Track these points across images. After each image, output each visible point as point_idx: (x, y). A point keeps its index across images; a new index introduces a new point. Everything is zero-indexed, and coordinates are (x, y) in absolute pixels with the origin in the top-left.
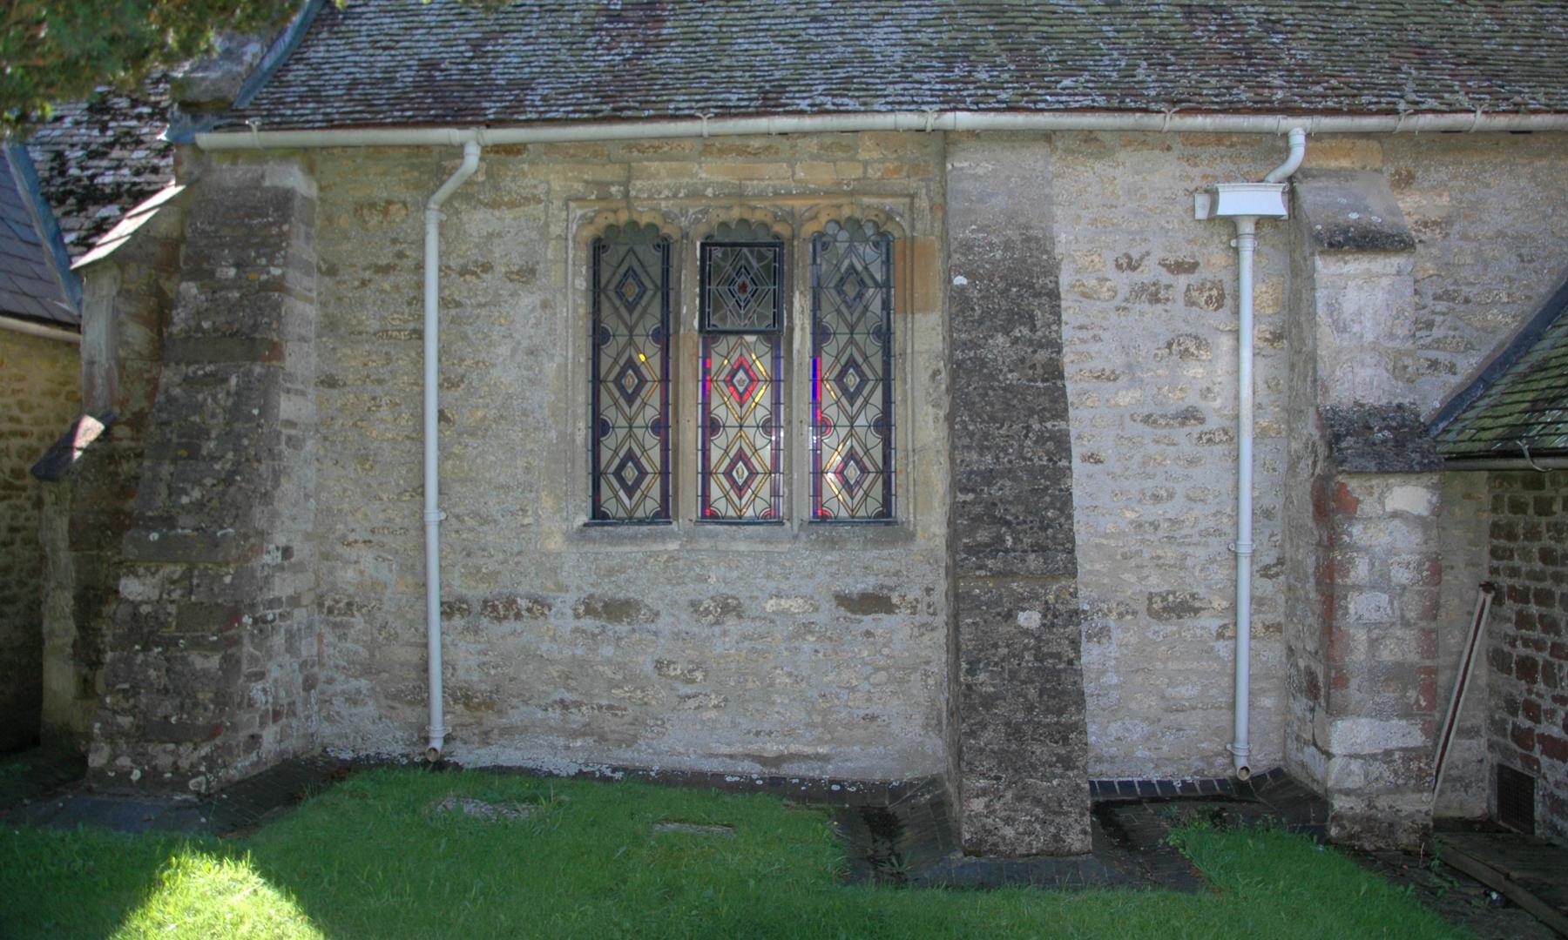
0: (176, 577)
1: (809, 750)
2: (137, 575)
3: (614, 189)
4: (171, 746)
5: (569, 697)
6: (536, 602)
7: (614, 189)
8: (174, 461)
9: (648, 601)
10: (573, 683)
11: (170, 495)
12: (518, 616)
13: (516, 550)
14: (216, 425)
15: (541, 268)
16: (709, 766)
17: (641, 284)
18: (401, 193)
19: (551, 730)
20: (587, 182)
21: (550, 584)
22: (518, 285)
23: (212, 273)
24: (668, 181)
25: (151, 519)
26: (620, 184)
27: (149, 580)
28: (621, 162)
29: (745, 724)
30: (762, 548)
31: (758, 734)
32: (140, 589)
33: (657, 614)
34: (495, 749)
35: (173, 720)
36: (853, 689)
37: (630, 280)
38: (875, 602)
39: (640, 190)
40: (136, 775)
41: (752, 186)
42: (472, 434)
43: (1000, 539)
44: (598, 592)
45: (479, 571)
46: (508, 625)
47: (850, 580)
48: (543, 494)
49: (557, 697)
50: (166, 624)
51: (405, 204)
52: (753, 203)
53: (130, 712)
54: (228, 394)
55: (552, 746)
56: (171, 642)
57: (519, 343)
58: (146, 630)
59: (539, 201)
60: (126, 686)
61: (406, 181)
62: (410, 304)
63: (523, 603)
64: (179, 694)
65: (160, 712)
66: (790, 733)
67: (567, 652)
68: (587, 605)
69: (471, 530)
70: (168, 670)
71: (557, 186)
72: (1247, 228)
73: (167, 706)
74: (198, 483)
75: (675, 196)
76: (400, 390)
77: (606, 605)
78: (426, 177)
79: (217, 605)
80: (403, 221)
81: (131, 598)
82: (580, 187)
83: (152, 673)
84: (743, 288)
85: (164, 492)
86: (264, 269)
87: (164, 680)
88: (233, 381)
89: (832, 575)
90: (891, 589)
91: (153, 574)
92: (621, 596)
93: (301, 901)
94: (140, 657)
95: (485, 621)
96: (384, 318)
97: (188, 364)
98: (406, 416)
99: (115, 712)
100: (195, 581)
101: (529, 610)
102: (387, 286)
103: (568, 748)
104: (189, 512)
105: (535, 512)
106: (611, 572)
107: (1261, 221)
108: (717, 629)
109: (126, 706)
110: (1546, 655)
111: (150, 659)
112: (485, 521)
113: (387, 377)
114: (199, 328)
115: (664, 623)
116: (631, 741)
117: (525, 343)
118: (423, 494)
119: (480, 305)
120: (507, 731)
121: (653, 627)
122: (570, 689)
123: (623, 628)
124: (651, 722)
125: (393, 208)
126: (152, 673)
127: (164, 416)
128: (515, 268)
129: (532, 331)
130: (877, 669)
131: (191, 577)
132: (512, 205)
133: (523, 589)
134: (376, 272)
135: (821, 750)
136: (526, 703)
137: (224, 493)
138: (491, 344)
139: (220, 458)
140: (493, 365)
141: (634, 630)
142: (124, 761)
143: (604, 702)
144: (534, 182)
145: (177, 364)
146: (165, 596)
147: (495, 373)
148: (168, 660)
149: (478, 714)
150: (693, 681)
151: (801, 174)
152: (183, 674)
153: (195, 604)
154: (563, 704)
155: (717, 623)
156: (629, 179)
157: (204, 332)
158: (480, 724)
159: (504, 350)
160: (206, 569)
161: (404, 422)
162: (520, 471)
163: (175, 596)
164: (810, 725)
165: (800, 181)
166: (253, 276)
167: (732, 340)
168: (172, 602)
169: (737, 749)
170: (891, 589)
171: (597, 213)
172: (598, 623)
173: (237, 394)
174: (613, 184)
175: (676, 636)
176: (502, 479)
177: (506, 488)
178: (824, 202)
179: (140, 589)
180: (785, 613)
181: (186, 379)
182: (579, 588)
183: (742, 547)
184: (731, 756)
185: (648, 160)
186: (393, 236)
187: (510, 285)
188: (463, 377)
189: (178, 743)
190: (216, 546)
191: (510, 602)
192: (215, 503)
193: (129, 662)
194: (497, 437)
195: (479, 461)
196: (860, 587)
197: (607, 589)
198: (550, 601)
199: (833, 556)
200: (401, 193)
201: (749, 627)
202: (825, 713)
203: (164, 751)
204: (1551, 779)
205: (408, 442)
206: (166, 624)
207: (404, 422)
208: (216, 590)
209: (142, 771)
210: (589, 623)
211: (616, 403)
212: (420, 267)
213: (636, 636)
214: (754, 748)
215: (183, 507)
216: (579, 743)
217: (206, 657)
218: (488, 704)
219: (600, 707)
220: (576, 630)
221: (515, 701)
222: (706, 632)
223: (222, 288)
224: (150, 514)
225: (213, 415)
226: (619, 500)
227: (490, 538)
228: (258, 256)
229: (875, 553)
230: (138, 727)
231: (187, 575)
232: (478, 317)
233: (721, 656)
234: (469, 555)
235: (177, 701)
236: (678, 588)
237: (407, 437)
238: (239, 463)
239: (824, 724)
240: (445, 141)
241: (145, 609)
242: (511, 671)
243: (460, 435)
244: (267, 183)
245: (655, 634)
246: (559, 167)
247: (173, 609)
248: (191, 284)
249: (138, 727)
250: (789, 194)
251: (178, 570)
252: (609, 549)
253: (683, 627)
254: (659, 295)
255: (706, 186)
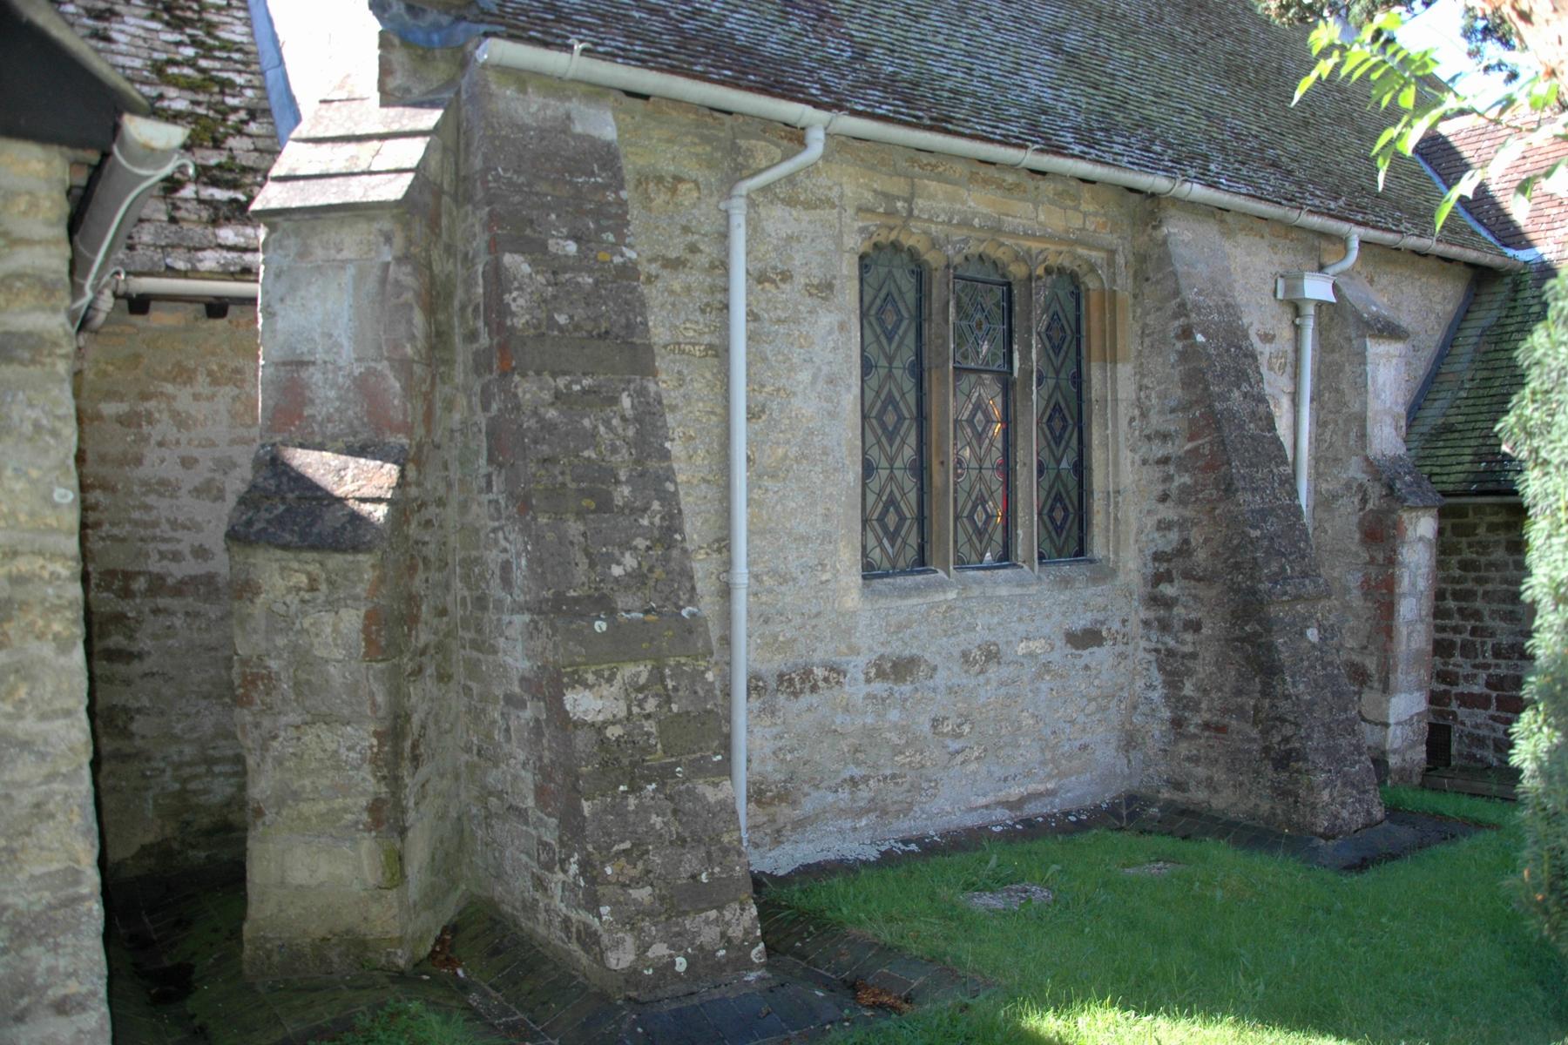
0: (642, 680)
1: (1041, 788)
2: (587, 686)
3: (899, 204)
4: (713, 914)
5: (857, 772)
6: (832, 669)
7: (899, 204)
8: (580, 514)
9: (927, 656)
10: (861, 756)
11: (592, 565)
12: (814, 689)
13: (814, 611)
14: (622, 461)
15: (837, 283)
16: (972, 820)
17: (898, 312)
18: (691, 169)
19: (842, 812)
20: (875, 191)
21: (843, 648)
22: (817, 301)
23: (544, 247)
24: (944, 204)
25: (576, 600)
26: (905, 200)
27: (605, 689)
28: (906, 176)
29: (998, 772)
30: (1018, 591)
31: (1006, 779)
32: (599, 704)
33: (935, 669)
34: (788, 847)
35: (704, 878)
36: (1072, 722)
37: (889, 307)
38: (1087, 638)
39: (921, 210)
40: (681, 964)
41: (1009, 223)
42: (773, 477)
43: (1283, 568)
44: (887, 650)
45: (776, 640)
46: (807, 699)
47: (1075, 618)
48: (841, 545)
49: (846, 775)
50: (649, 749)
51: (696, 182)
52: (1002, 239)
53: (644, 879)
54: (624, 419)
55: (841, 831)
56: (664, 774)
57: (819, 369)
58: (626, 761)
59: (833, 206)
60: (627, 845)
61: (697, 155)
62: (703, 311)
63: (819, 672)
64: (700, 841)
65: (685, 870)
66: (1029, 775)
67: (859, 722)
68: (878, 667)
69: (770, 591)
70: (675, 812)
71: (849, 191)
72: (1310, 310)
73: (691, 862)
74: (626, 545)
75: (950, 221)
76: (697, 420)
77: (895, 665)
78: (719, 155)
79: (709, 712)
80: (694, 206)
81: (589, 719)
82: (869, 196)
83: (656, 820)
84: (979, 325)
85: (584, 563)
86: (614, 248)
87: (675, 828)
88: (626, 402)
89: (1064, 614)
90: (1103, 623)
91: (610, 680)
92: (907, 653)
93: (1281, 1025)
94: (632, 802)
95: (781, 699)
96: (677, 327)
97: (554, 375)
98: (701, 453)
99: (624, 886)
100: (670, 684)
101: (826, 680)
102: (677, 286)
103: (855, 829)
104: (627, 587)
105: (834, 567)
106: (900, 628)
107: (1320, 304)
108: (981, 678)
109: (634, 873)
110: (1466, 636)
111: (648, 802)
112: (784, 579)
113: (680, 402)
114: (553, 324)
115: (941, 678)
116: (907, 809)
117: (825, 369)
118: (728, 548)
119: (779, 321)
120: (799, 824)
121: (931, 683)
122: (858, 764)
123: (906, 688)
124: (925, 785)
125: (683, 187)
126: (656, 820)
127: (545, 449)
128: (816, 281)
129: (831, 357)
130: (1090, 701)
131: (662, 679)
132: (808, 206)
133: (817, 657)
134: (664, 266)
135: (1050, 786)
136: (817, 787)
137: (666, 559)
138: (792, 369)
139: (645, 510)
140: (795, 394)
141: (916, 689)
142: (659, 950)
143: (888, 772)
144: (830, 183)
145: (538, 373)
146: (635, 710)
147: (796, 402)
148: (670, 798)
149: (772, 810)
150: (960, 735)
151: (1042, 218)
152: (697, 815)
153: (678, 715)
154: (853, 782)
155: (982, 672)
156: (913, 196)
157: (561, 329)
158: (773, 821)
159: (804, 376)
160: (679, 664)
161: (699, 462)
162: (819, 519)
163: (651, 705)
164: (1043, 763)
165: (1040, 223)
166: (603, 256)
167: (973, 378)
168: (648, 717)
169: (990, 798)
170: (1103, 623)
171: (879, 227)
172: (886, 686)
173: (638, 419)
174: (898, 198)
175: (950, 690)
176: (802, 529)
177: (805, 539)
178: (1052, 248)
179: (599, 704)
180: (1031, 655)
181: (558, 395)
182: (871, 649)
183: (1003, 591)
184: (987, 807)
185: (928, 178)
186: (684, 222)
187: (808, 300)
188: (764, 406)
189: (720, 908)
190: (690, 632)
191: (807, 673)
192: (658, 572)
193: (618, 810)
194: (799, 479)
195: (779, 507)
196: (1082, 622)
197: (896, 648)
198: (844, 667)
199: (1064, 596)
200: (691, 169)
201: (1006, 672)
202: (1055, 747)
203: (707, 922)
204: (1468, 722)
205: (703, 486)
206: (649, 749)
207: (699, 462)
208: (701, 693)
209: (686, 956)
210: (879, 687)
211: (879, 442)
212: (722, 266)
213: (919, 695)
214: (1002, 795)
215: (617, 580)
216: (864, 822)
217: (716, 785)
218: (783, 797)
219: (885, 778)
220: (868, 696)
221: (806, 788)
222: (973, 683)
223: (565, 269)
224: (572, 593)
225: (614, 450)
226: (883, 549)
227: (788, 599)
228: (601, 229)
229: (1092, 590)
230: (662, 899)
231: (658, 676)
232: (777, 333)
233: (984, 706)
234: (766, 622)
235: (702, 853)
236: (953, 640)
237: (704, 480)
238: (672, 517)
239: (1053, 760)
240: (791, 119)
241: (613, 732)
242: (804, 753)
243: (760, 476)
244: (578, 128)
245: (934, 690)
246: (851, 170)
247: (650, 726)
248: (518, 258)
249: (662, 899)
250: (1034, 236)
251: (643, 671)
252: (899, 602)
253: (955, 680)
254: (914, 324)
255: (975, 215)
